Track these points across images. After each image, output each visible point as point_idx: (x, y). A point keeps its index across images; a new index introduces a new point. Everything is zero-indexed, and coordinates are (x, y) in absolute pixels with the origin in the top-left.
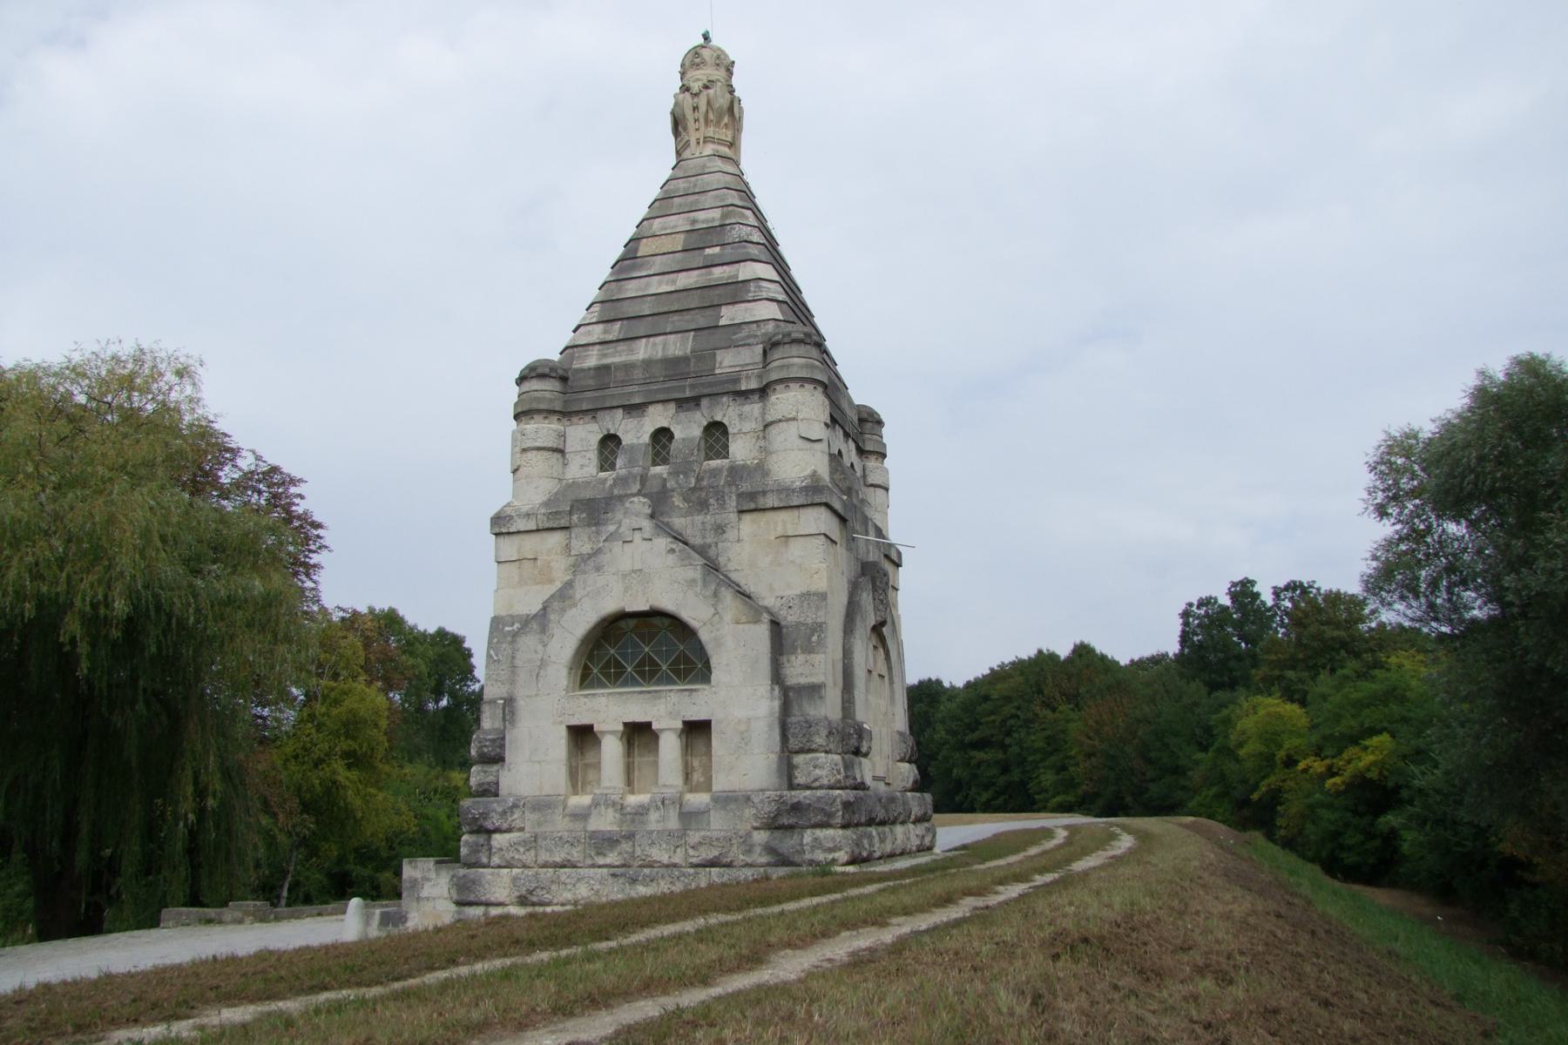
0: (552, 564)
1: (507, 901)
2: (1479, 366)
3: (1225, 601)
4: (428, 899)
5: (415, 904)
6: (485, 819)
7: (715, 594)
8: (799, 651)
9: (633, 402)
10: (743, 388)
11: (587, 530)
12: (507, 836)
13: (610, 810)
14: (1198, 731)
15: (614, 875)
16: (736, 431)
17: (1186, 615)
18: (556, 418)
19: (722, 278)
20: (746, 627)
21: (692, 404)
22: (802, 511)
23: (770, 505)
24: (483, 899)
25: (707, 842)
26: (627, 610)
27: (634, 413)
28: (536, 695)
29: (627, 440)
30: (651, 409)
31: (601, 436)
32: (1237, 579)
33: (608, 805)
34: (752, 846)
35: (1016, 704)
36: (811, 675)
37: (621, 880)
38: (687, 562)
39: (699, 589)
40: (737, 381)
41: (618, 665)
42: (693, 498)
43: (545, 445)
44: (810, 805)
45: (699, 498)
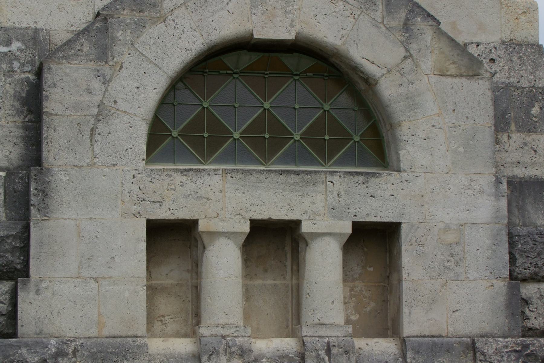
7: (406, 27)
8: (513, 127)
20: (457, 80)
26: (256, 36)
28: (91, 165)
33: (232, 354)
36: (534, 164)
39: (378, 15)
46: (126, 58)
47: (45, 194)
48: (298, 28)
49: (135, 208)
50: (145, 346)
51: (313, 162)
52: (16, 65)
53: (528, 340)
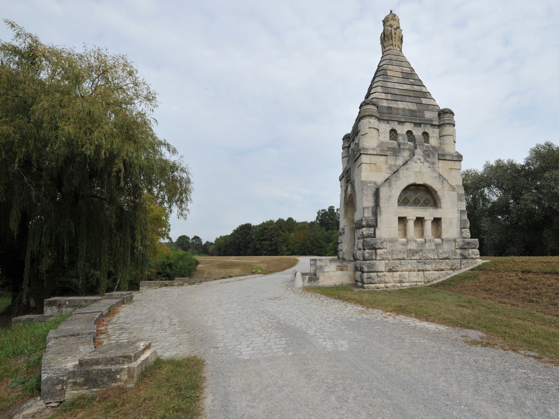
0: (382, 166)
1: (384, 270)
2: (487, 160)
3: (327, 210)
4: (327, 272)
5: (322, 273)
6: (375, 245)
7: (442, 182)
9: (401, 120)
10: (434, 124)
11: (393, 157)
12: (382, 250)
13: (414, 243)
14: (325, 239)
15: (419, 262)
16: (431, 136)
17: (318, 213)
18: (375, 118)
19: (417, 90)
20: (451, 192)
21: (418, 125)
22: (456, 162)
23: (448, 159)
24: (377, 270)
25: (444, 252)
26: (417, 183)
27: (400, 124)
28: (388, 207)
29: (399, 132)
30: (406, 124)
31: (390, 129)
32: (330, 206)
34: (457, 253)
35: (275, 231)
37: (422, 263)
38: (434, 171)
40: (432, 121)
41: (408, 200)
42: (426, 153)
43: (376, 127)
44: (471, 243)
45: (427, 153)
46: (394, 187)
47: (380, 211)
48: (424, 182)
49: (396, 214)
50: (398, 240)
51: (424, 206)
52: (372, 188)
53: (464, 239)
